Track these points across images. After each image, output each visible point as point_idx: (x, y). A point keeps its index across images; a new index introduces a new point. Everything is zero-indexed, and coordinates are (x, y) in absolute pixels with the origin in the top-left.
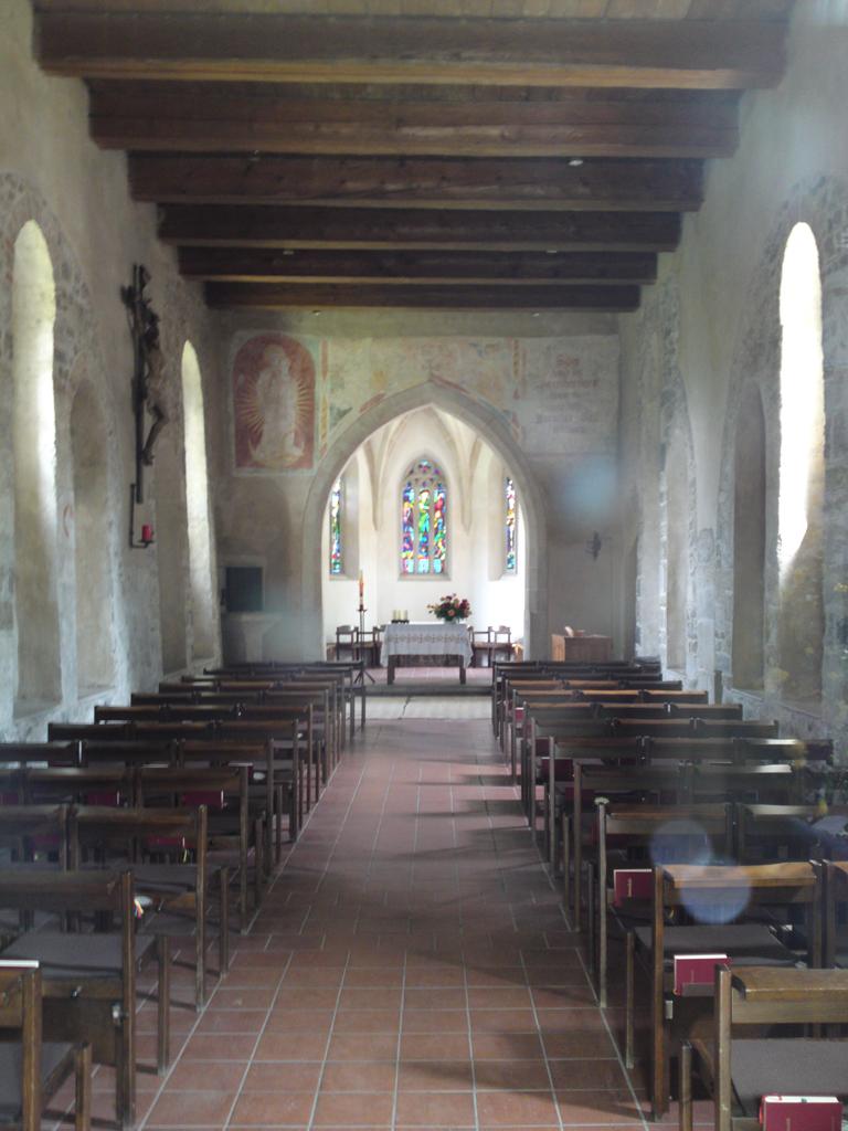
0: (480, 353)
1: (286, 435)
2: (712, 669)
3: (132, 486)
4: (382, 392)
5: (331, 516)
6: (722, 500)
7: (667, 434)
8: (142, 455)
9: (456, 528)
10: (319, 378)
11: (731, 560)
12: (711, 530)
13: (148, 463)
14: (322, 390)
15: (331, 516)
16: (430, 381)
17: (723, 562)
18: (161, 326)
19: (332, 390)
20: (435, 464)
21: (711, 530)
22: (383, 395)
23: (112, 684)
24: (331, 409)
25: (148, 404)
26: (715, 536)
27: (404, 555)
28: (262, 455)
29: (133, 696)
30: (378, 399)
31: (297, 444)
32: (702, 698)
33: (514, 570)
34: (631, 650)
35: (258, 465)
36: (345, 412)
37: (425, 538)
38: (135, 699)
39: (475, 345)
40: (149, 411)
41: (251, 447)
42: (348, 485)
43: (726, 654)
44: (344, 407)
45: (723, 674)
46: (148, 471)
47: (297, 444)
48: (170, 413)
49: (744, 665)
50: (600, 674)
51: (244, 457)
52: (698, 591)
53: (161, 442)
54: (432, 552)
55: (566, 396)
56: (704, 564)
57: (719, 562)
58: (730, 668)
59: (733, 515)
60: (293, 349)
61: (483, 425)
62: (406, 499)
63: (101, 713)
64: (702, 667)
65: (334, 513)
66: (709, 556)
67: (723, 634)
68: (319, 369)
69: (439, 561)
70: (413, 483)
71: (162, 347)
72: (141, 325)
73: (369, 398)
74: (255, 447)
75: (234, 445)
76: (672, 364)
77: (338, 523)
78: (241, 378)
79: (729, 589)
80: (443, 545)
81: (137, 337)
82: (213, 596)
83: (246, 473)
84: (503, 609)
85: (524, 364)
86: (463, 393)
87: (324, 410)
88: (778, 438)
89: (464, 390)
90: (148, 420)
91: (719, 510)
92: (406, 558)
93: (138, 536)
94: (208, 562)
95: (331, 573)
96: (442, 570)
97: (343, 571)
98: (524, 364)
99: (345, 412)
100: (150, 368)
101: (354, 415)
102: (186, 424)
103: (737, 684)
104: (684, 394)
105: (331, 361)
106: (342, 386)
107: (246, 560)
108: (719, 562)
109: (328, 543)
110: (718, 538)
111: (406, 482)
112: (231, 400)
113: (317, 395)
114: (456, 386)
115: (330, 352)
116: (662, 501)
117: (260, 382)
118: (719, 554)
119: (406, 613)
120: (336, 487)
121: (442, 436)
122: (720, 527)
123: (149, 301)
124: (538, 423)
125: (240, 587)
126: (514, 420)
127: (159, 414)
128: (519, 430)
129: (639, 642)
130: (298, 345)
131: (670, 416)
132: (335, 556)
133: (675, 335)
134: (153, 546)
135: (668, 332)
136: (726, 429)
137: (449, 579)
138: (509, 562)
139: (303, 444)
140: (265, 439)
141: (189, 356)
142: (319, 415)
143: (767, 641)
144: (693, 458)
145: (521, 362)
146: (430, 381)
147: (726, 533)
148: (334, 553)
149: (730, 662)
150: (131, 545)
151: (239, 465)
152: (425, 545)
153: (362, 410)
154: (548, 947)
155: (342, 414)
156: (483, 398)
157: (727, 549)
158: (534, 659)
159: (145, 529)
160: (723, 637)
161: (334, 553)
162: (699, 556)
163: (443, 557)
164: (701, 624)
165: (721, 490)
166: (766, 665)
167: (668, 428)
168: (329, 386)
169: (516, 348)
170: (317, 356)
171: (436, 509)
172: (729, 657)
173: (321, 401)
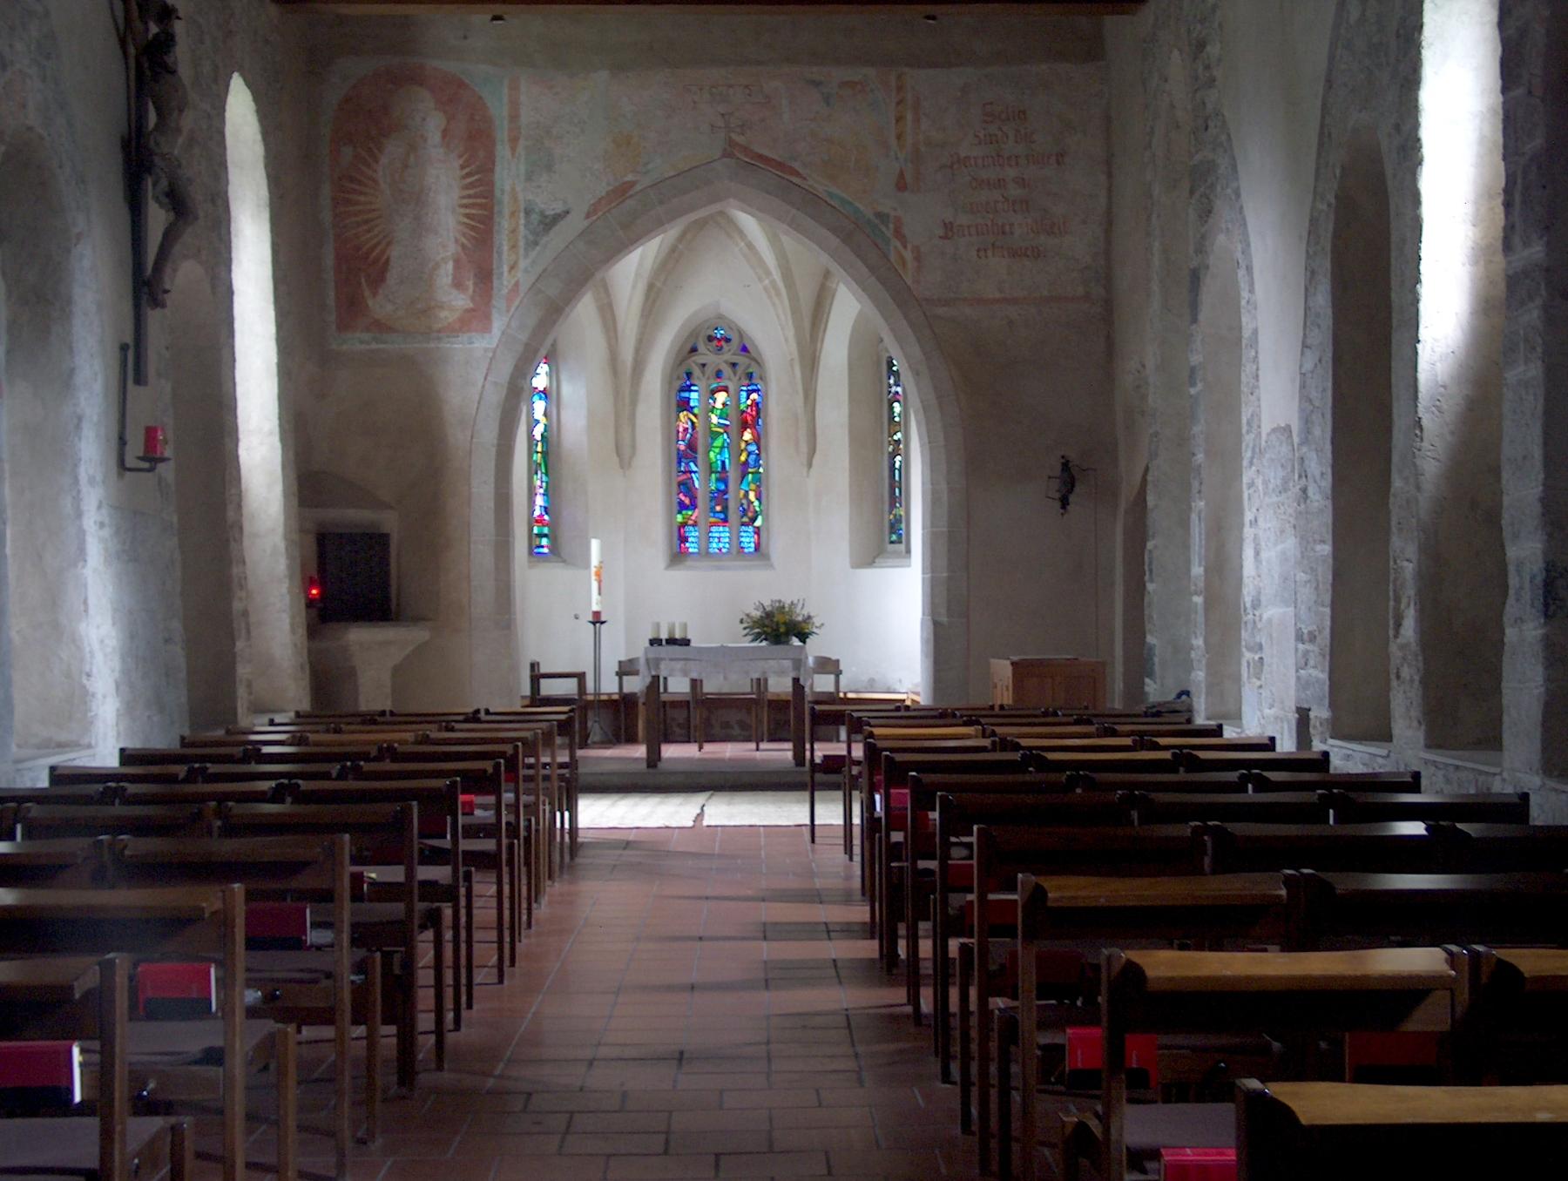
0: (827, 100)
1: (437, 266)
2: (1291, 705)
3: (124, 348)
4: (630, 178)
5: (531, 436)
6: (1309, 366)
7: (1201, 249)
8: (145, 287)
9: (779, 460)
10: (502, 151)
11: (1327, 483)
12: (1289, 426)
13: (157, 303)
14: (509, 176)
15: (531, 436)
16: (727, 154)
17: (1310, 492)
18: (179, 27)
19: (529, 178)
20: (741, 334)
21: (1289, 426)
22: (632, 184)
23: (85, 741)
24: (528, 212)
25: (154, 185)
26: (1296, 440)
27: (680, 518)
28: (389, 307)
29: (122, 750)
30: (622, 192)
31: (458, 284)
32: (1271, 744)
33: (902, 547)
34: (1135, 689)
35: (381, 327)
36: (557, 218)
37: (711, 496)
38: (126, 756)
39: (817, 84)
40: (157, 200)
41: (367, 293)
42: (563, 377)
43: (1319, 674)
44: (559, 207)
45: (1312, 714)
46: (154, 317)
47: (458, 284)
48: (197, 194)
49: (1355, 699)
50: (1070, 719)
51: (351, 309)
52: (1264, 555)
53: (184, 275)
54: (733, 515)
55: (1000, 183)
56: (1275, 499)
57: (1304, 490)
58: (1327, 702)
59: (1329, 393)
60: (453, 94)
61: (835, 241)
62: (684, 405)
63: (57, 775)
64: (1271, 707)
65: (538, 432)
66: (1285, 481)
67: (1310, 633)
68: (502, 134)
69: (750, 529)
70: (697, 372)
71: (185, 71)
72: (138, 24)
73: (602, 189)
74: (375, 295)
75: (336, 281)
76: (1209, 106)
77: (545, 454)
78: (347, 152)
79: (1323, 542)
80: (758, 498)
81: (132, 51)
82: (290, 567)
83: (356, 342)
84: (887, 634)
85: (917, 120)
86: (795, 180)
87: (513, 214)
88: (1416, 227)
89: (798, 174)
90: (157, 218)
91: (1303, 386)
92: (683, 525)
93: (136, 447)
94: (282, 519)
95: (531, 553)
96: (757, 547)
97: (555, 549)
98: (917, 120)
99: (557, 218)
100: (160, 114)
101: (575, 223)
102: (234, 240)
103: (1338, 731)
104: (1234, 168)
105: (526, 116)
106: (549, 168)
107: (355, 516)
108: (1304, 490)
109: (528, 496)
110: (1300, 444)
111: (682, 372)
112: (327, 190)
113: (498, 184)
114: (781, 166)
115: (523, 98)
116: (1193, 384)
117: (384, 160)
118: (1304, 475)
119: (685, 626)
120: (540, 381)
121: (746, 269)
122: (1307, 422)
123: (166, 292)
124: (945, 237)
125: (354, 576)
126: (898, 233)
127: (178, 203)
128: (908, 255)
129: (1151, 675)
130: (462, 85)
131: (1206, 213)
132: (540, 521)
133: (1213, 50)
134: (167, 471)
135: (1201, 45)
136: (1313, 222)
137: (771, 566)
138: (896, 530)
139: (470, 284)
140: (392, 277)
141: (241, 110)
142: (504, 224)
143: (1396, 636)
144: (1252, 291)
145: (909, 116)
146: (727, 154)
147: (1317, 432)
148: (537, 513)
149: (1327, 688)
150: (122, 466)
151: (343, 326)
152: (720, 497)
153: (588, 216)
154: (971, 897)
155: (549, 222)
156: (834, 190)
157: (1319, 466)
158: (944, 705)
159: (151, 433)
160: (1312, 638)
161: (537, 513)
162: (1266, 483)
163: (758, 523)
164: (1270, 621)
165: (1305, 346)
166: (1394, 683)
167: (1203, 237)
168: (522, 168)
169: (900, 89)
170: (498, 109)
171: (744, 426)
172: (1324, 676)
173: (506, 198)
